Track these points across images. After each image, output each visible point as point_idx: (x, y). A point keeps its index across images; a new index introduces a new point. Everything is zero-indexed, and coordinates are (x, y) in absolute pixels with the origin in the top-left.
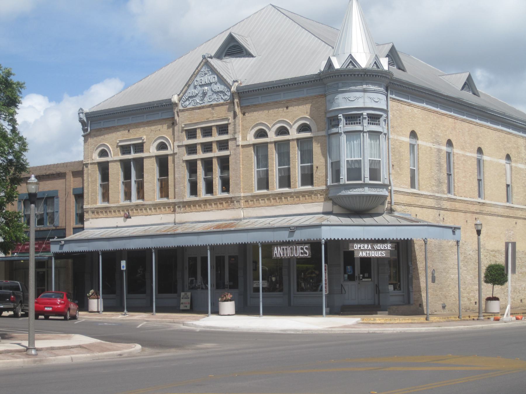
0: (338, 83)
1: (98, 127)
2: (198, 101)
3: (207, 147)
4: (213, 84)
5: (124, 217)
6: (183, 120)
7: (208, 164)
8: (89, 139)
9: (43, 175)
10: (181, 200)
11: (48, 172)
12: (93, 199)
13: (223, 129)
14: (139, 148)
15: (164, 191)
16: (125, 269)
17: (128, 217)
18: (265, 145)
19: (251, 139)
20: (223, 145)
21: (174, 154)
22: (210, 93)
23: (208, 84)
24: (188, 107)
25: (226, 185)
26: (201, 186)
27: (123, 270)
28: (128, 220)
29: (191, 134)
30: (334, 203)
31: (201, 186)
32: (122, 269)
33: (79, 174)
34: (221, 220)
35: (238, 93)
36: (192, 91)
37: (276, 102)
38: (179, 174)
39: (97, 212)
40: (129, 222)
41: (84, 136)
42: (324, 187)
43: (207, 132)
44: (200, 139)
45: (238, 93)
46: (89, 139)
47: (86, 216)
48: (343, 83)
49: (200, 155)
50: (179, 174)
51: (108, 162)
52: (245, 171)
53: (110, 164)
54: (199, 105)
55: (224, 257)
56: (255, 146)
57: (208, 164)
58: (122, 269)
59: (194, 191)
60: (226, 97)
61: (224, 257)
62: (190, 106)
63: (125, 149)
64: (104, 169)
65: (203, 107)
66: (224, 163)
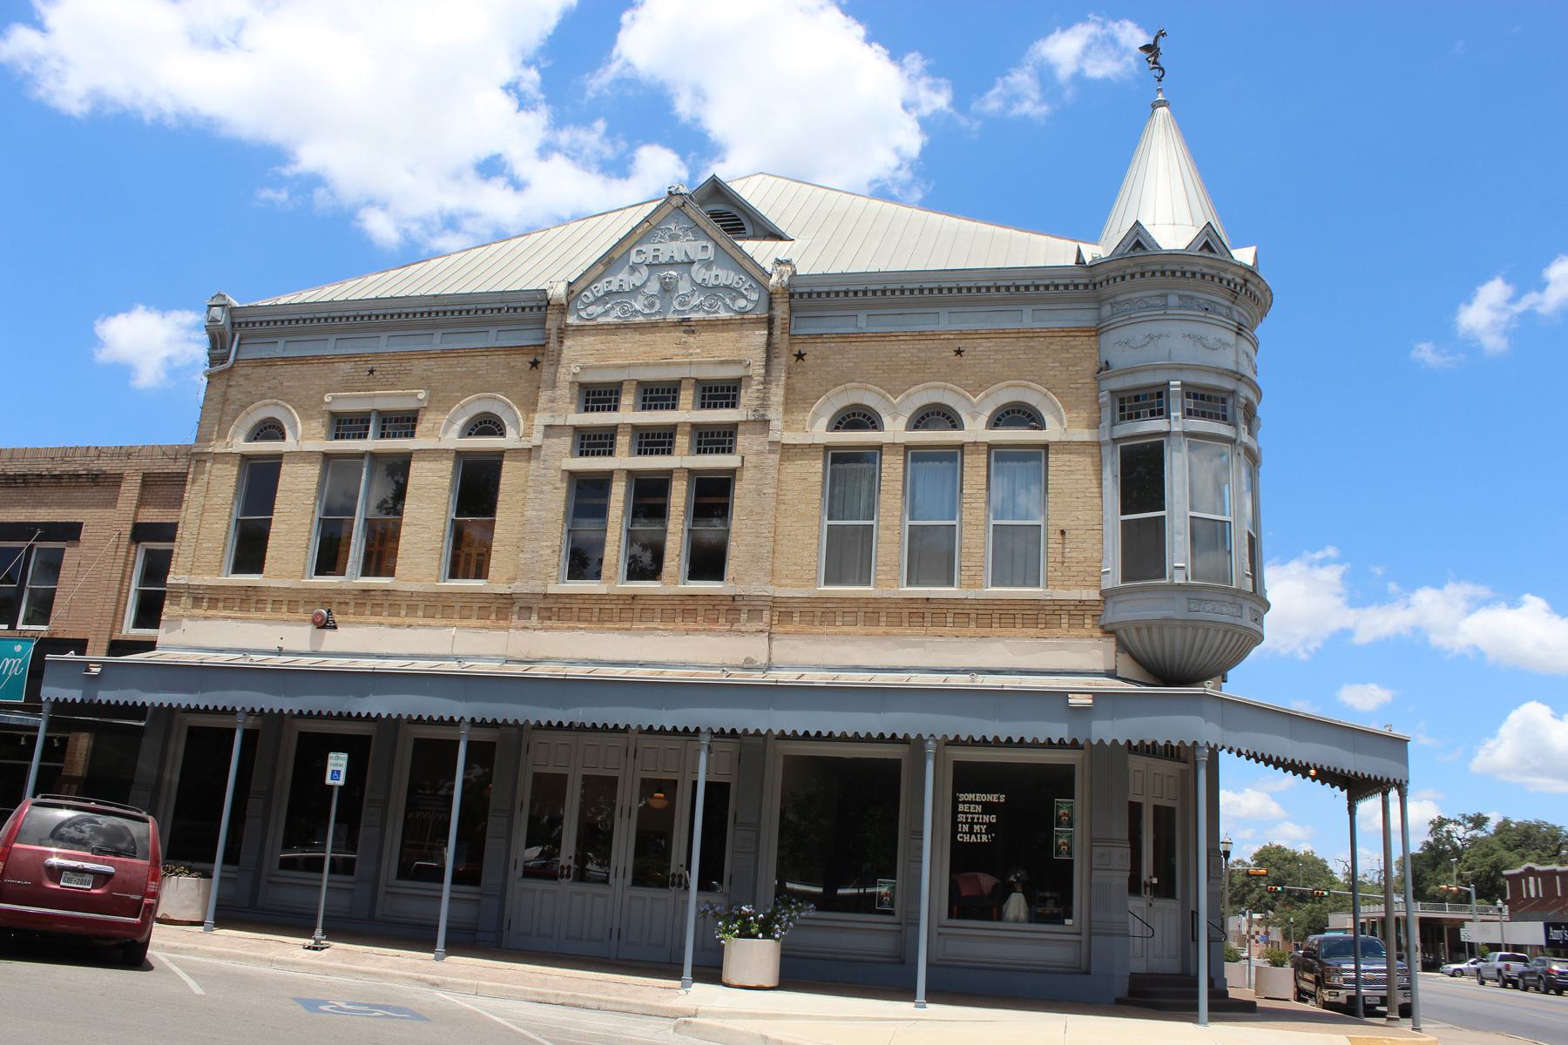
0: (1166, 296)
1: (264, 355)
2: (637, 307)
3: (655, 440)
4: (695, 267)
5: (314, 622)
6: (581, 358)
7: (649, 496)
8: (1330, 575)
9: (40, 476)
10: (538, 590)
11: (44, 467)
12: (201, 554)
13: (720, 393)
14: (404, 423)
15: (468, 555)
16: (341, 782)
17: (325, 624)
18: (867, 457)
19: (820, 432)
20: (715, 439)
21: (529, 453)
22: (684, 287)
23: (683, 263)
24: (601, 320)
25: (707, 562)
26: (615, 551)
27: (332, 787)
28: (328, 633)
29: (599, 396)
30: (1122, 647)
31: (615, 551)
32: (329, 781)
33: (165, 484)
34: (685, 665)
35: (791, 296)
36: (622, 279)
37: (921, 333)
38: (531, 513)
39: (209, 599)
40: (332, 640)
41: (209, 376)
42: (1094, 595)
43: (659, 394)
44: (628, 414)
45: (791, 296)
46: (1330, 575)
47: (168, 609)
48: (1181, 297)
49: (623, 460)
50: (531, 513)
51: (279, 457)
52: (778, 524)
53: (284, 468)
54: (640, 319)
55: (563, 779)
56: (839, 457)
57: (649, 496)
58: (329, 781)
59: (582, 562)
60: (742, 303)
61: (563, 779)
62: (610, 319)
63: (345, 424)
64: (260, 481)
65: (653, 327)
66: (713, 496)
